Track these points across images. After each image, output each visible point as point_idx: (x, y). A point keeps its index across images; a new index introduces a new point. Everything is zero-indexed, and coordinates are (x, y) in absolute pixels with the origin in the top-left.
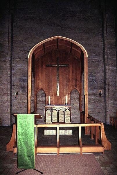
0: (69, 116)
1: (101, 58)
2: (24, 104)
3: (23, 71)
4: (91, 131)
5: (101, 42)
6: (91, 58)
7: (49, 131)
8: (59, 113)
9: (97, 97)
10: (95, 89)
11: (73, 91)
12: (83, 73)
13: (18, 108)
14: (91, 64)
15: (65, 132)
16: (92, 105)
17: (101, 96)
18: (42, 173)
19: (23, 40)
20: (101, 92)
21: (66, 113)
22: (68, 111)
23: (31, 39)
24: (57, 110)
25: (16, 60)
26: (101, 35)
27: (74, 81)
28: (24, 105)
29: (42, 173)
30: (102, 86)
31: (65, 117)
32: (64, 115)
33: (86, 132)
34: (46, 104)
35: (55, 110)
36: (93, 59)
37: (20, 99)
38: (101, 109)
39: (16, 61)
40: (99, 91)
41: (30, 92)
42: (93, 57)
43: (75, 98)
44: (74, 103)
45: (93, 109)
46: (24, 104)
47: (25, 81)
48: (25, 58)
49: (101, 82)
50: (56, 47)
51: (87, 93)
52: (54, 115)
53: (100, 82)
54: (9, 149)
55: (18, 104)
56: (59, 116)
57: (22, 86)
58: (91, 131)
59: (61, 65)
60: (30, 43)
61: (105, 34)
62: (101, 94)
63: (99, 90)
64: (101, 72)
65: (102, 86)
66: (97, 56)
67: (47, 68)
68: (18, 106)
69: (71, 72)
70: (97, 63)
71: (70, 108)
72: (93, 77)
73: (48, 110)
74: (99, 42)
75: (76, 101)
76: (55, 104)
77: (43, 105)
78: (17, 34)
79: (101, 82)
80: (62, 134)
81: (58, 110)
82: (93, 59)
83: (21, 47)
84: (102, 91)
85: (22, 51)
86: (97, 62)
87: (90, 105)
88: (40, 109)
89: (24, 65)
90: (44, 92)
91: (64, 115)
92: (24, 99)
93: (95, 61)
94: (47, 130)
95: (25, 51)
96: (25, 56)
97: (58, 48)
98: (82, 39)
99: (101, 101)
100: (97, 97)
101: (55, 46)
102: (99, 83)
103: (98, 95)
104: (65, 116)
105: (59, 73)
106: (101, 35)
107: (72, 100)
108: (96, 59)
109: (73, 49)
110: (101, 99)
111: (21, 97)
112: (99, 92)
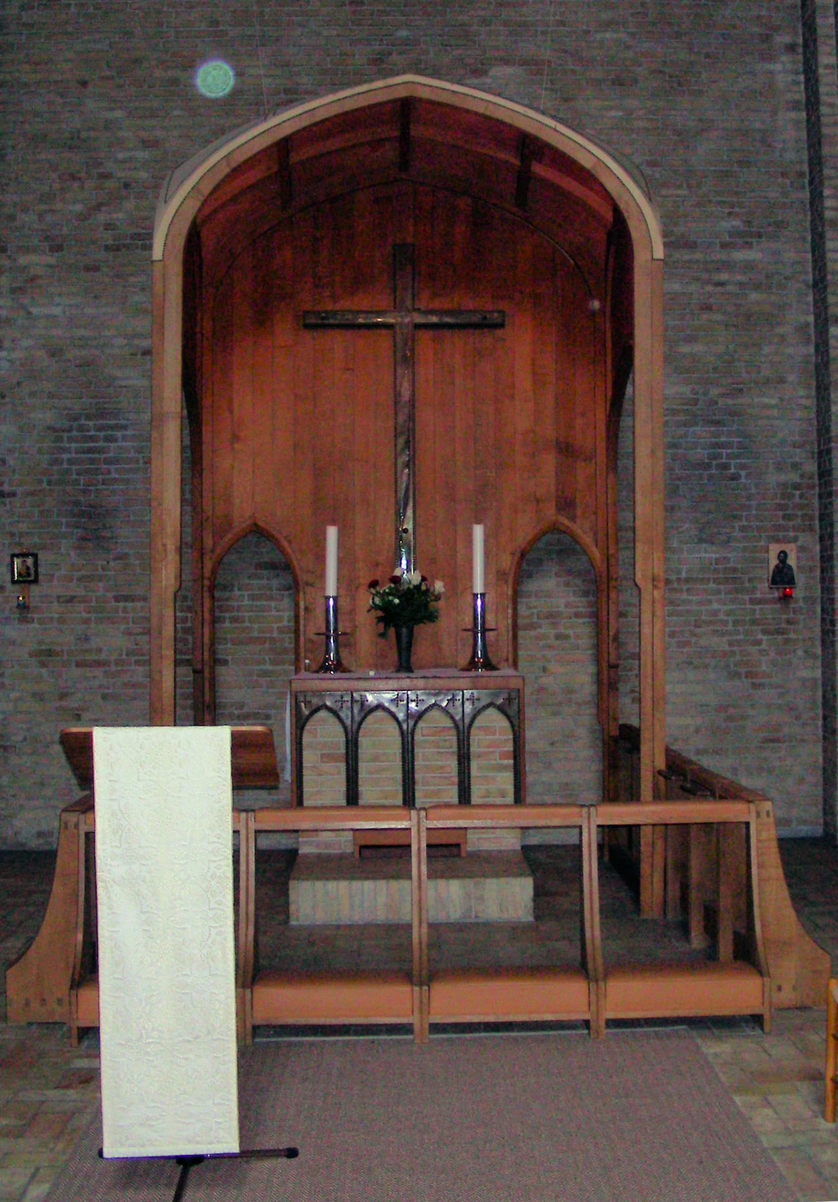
0: (503, 768)
1: (789, 256)
2: (99, 664)
3: (87, 364)
4: (685, 888)
5: (792, 115)
6: (699, 256)
7: (331, 885)
8: (418, 737)
9: (760, 601)
10: (737, 534)
11: (541, 544)
12: (372, 673)
13: (39, 696)
14: (708, 308)
15: (468, 895)
16: (712, 676)
17: (786, 598)
18: (292, 1153)
19: (84, 84)
20: (792, 561)
21: (478, 742)
22: (495, 720)
23: (159, 73)
24: (401, 716)
25: (23, 260)
26: (791, 48)
27: (549, 462)
28: (98, 672)
29: (292, 1153)
30: (801, 507)
31: (474, 772)
32: (464, 758)
33: (645, 896)
34: (297, 659)
35: (379, 714)
36: (726, 266)
37: (61, 621)
38: (791, 708)
39: (24, 269)
40: (774, 550)
41: (172, 557)
42: (724, 246)
43: (559, 613)
44: (549, 654)
45: (721, 708)
46: (99, 664)
47: (100, 451)
48: (107, 248)
49: (795, 466)
50: (390, 152)
51: (659, 570)
52: (375, 759)
53: (779, 467)
54: (27, 1004)
55: (43, 665)
56: (418, 764)
57: (77, 503)
58: (685, 888)
59: (434, 319)
60: (153, 114)
61: (822, 49)
62: (791, 581)
63: (778, 541)
64: (791, 378)
65: (801, 507)
66: (759, 236)
67: (309, 335)
68: (39, 679)
69: (524, 381)
70: (754, 296)
71: (509, 700)
72: (717, 423)
73: (323, 714)
74: (774, 112)
75: (566, 637)
76: (375, 667)
77: (266, 673)
78: (31, 26)
79: (795, 466)
80: (441, 918)
81: (408, 715)
82: (726, 266)
83: (74, 143)
84: (802, 549)
85: (74, 177)
86: (757, 287)
87: (691, 675)
88: (241, 706)
89: (88, 311)
90: (282, 551)
91: (464, 758)
92: (99, 621)
93: (741, 284)
94: (319, 884)
95: (109, 184)
96: (108, 226)
97: (404, 164)
98: (618, 82)
99: (787, 641)
100: (760, 601)
101: (377, 144)
102: (773, 478)
103: (763, 588)
104: (474, 765)
105: (413, 383)
106: (791, 48)
107: (532, 626)
108: (749, 266)
109: (543, 180)
110: (788, 622)
111: (71, 600)
112: (774, 562)
